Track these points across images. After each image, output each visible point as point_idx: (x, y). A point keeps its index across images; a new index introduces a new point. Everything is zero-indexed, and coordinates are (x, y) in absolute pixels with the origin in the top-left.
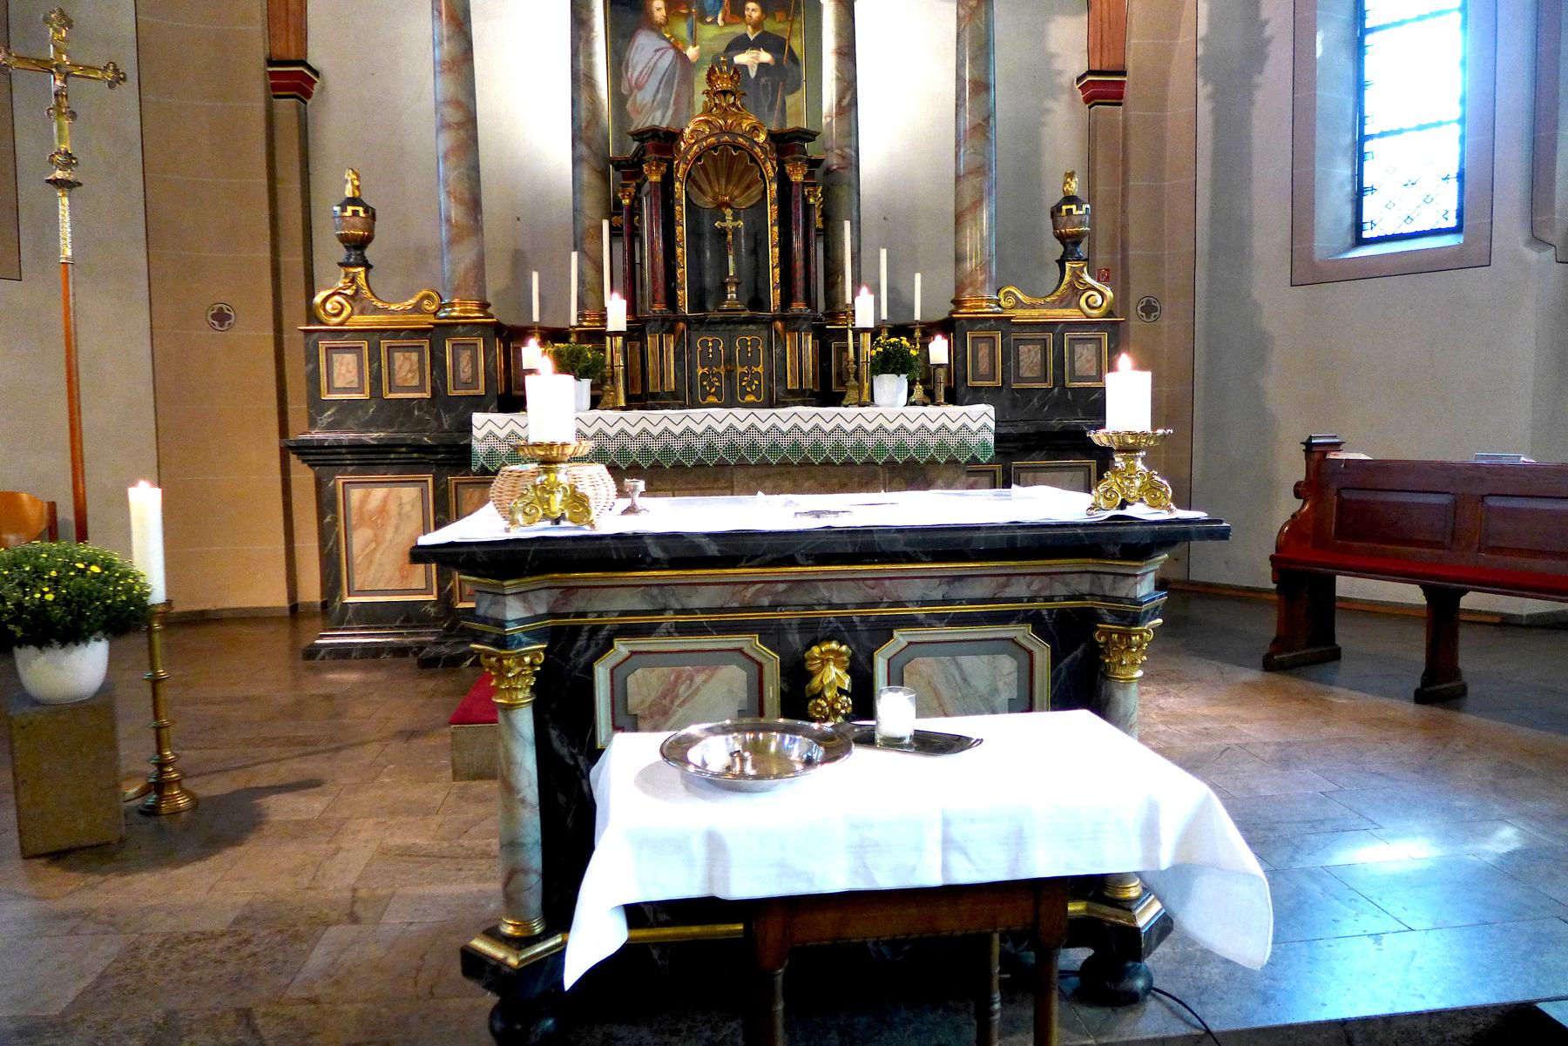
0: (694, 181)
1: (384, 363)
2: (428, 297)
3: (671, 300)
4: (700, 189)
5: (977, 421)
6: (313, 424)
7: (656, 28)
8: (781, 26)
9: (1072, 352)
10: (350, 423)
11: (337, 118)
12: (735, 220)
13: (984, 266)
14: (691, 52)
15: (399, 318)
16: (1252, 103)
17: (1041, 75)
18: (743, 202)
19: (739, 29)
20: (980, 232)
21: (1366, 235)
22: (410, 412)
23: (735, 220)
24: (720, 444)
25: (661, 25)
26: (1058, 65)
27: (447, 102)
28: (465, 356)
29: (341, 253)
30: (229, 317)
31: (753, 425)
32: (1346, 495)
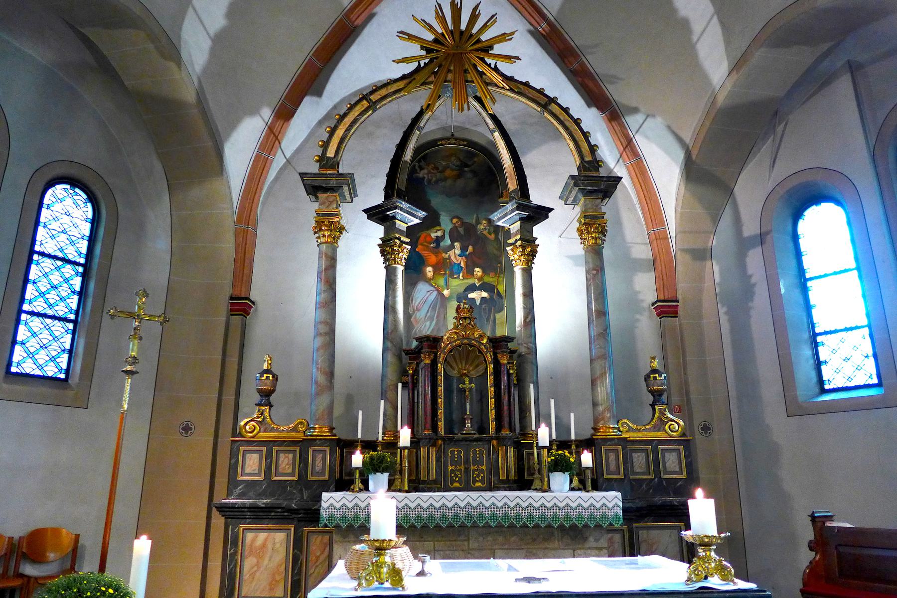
0: (448, 363)
1: (274, 459)
2: (301, 423)
3: (435, 428)
4: (451, 367)
5: (610, 501)
6: (229, 495)
7: (428, 281)
8: (491, 280)
9: (663, 457)
10: (251, 494)
11: (261, 326)
12: (470, 383)
13: (609, 409)
14: (446, 293)
15: (285, 434)
16: (749, 317)
17: (632, 302)
18: (474, 374)
19: (470, 281)
20: (604, 390)
21: (827, 387)
22: (285, 488)
23: (470, 383)
24: (462, 514)
25: (430, 279)
26: (641, 297)
27: (321, 323)
28: (319, 457)
29: (257, 398)
30: (191, 429)
31: (481, 503)
32: (841, 549)
